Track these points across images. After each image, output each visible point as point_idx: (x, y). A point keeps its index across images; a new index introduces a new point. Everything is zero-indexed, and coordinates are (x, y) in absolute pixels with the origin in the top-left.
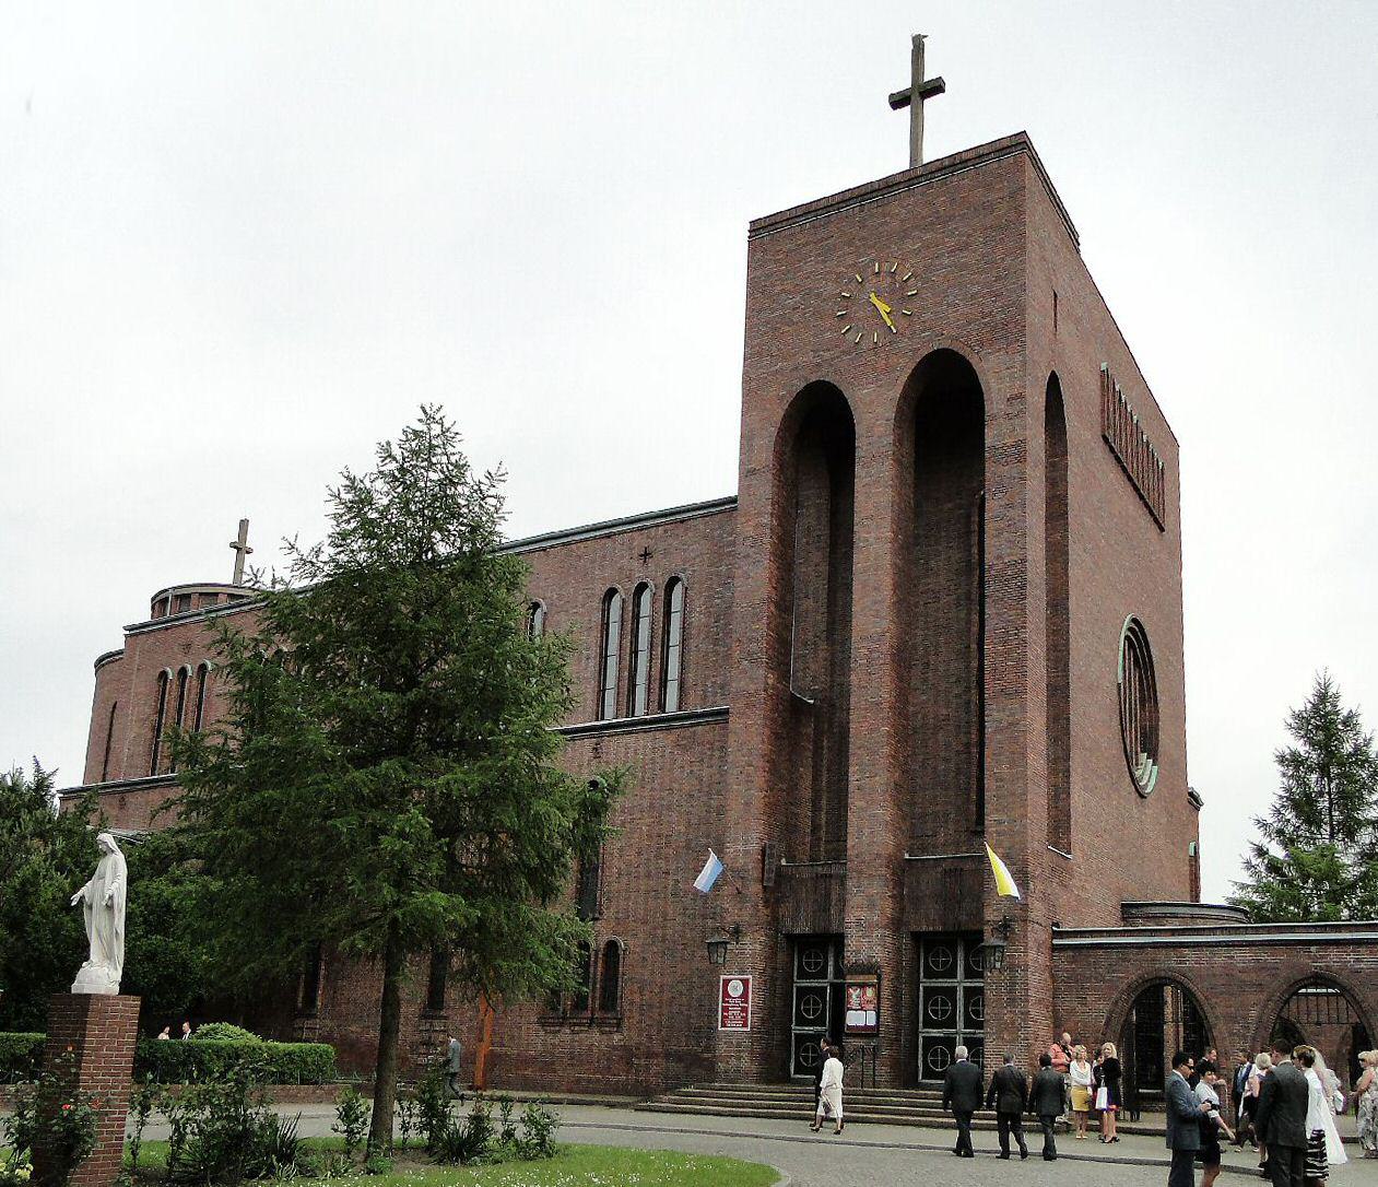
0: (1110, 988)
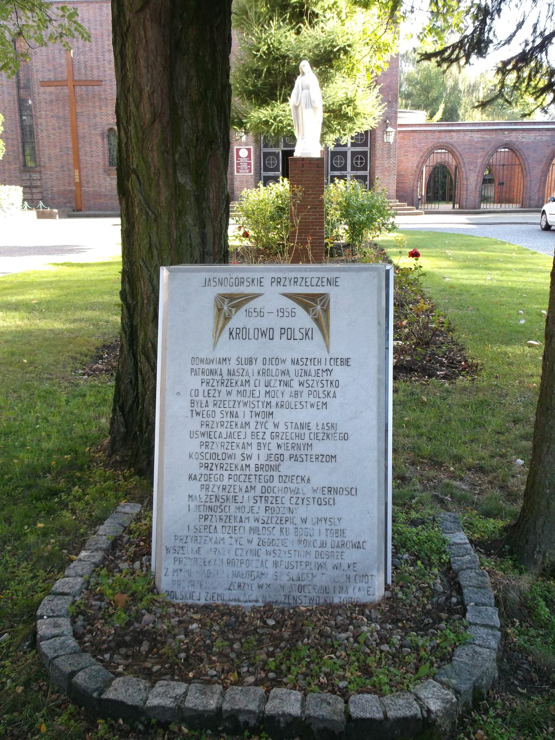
0: (419, 150)
